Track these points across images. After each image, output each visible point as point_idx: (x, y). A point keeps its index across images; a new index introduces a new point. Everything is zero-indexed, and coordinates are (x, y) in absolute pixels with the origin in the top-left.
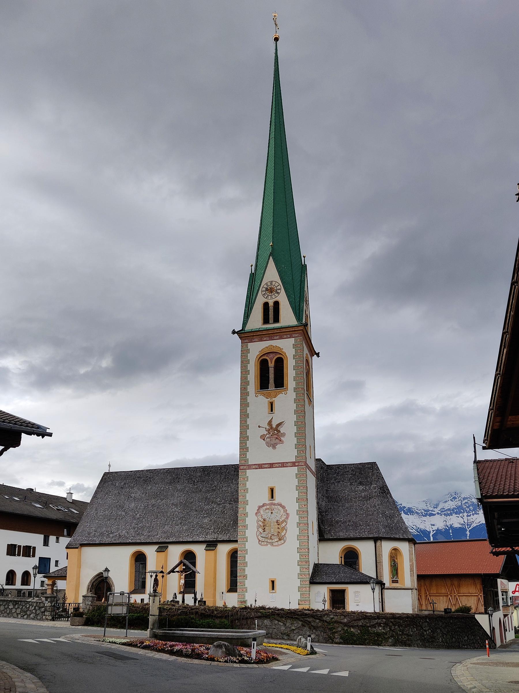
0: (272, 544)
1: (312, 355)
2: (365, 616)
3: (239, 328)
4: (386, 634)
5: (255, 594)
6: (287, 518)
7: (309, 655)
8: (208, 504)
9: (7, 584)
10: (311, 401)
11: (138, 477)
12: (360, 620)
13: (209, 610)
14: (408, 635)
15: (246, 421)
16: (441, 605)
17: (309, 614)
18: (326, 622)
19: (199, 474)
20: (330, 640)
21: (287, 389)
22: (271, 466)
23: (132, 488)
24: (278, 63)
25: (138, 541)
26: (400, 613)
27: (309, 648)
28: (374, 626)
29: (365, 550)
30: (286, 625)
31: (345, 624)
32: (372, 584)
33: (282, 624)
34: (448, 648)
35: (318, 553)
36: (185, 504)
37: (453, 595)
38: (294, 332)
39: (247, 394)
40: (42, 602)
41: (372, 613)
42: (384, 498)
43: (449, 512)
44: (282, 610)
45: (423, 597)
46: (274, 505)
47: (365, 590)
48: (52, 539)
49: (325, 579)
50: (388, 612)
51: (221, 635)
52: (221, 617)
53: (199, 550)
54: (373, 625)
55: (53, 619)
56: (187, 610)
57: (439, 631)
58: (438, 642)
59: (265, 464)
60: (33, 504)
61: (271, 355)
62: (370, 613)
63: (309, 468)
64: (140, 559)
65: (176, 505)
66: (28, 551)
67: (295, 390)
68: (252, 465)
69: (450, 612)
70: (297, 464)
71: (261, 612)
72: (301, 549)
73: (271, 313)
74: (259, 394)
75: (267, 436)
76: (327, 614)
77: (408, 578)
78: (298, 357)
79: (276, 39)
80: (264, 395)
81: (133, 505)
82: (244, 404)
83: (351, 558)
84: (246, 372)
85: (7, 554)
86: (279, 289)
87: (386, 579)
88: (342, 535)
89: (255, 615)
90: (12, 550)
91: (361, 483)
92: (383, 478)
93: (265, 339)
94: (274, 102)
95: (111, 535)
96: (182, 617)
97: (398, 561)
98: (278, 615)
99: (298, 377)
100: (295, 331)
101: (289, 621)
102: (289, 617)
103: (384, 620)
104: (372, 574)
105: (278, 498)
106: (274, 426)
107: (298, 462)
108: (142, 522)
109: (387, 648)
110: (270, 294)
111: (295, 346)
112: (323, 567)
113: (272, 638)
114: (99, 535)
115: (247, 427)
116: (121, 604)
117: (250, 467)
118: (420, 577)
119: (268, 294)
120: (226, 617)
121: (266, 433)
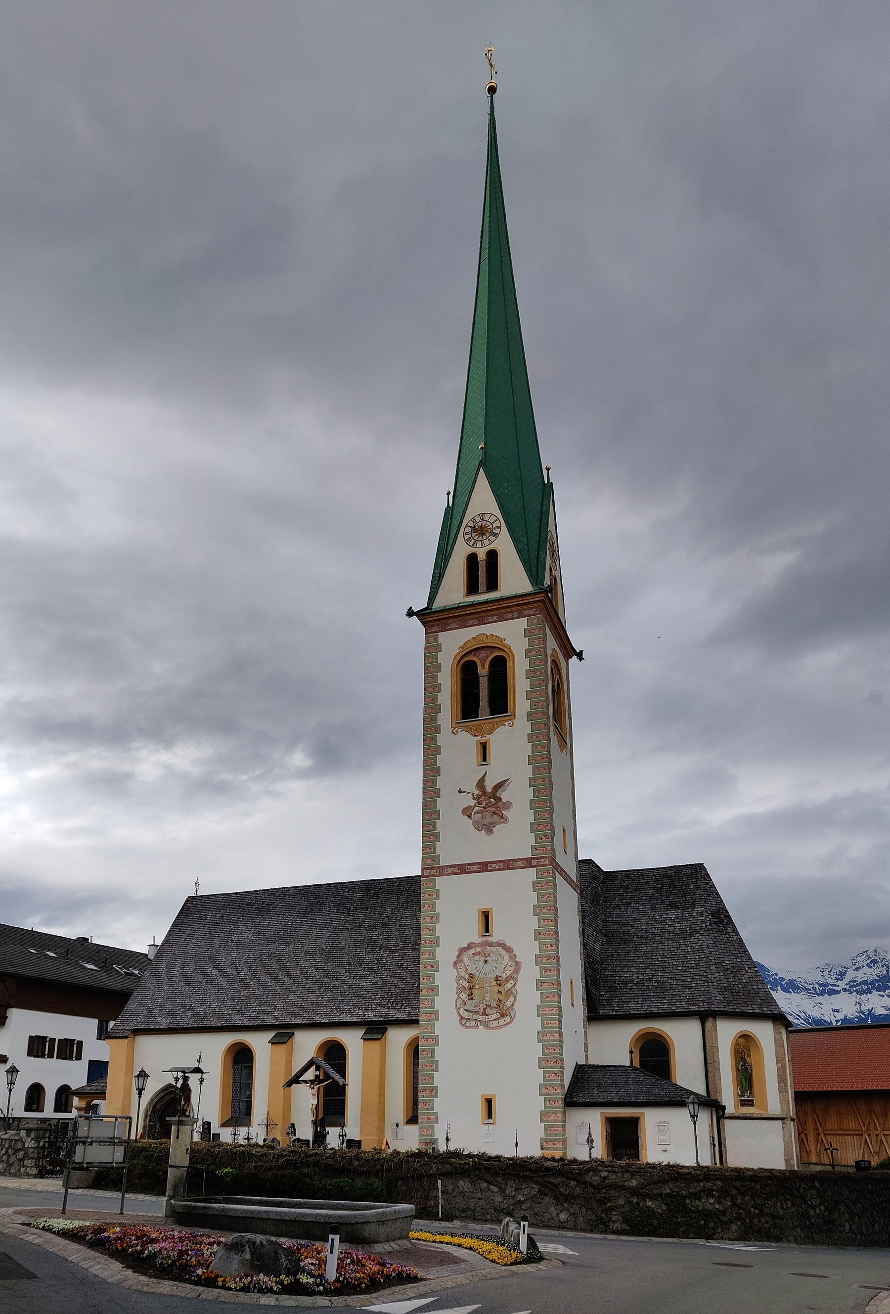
0: (487, 1025)
1: (568, 657)
2: (678, 1173)
3: (420, 604)
4: (724, 1213)
5: (460, 1130)
6: (517, 971)
7: (520, 1263)
8: (373, 951)
9: (28, 1109)
10: (565, 742)
11: (247, 904)
12: (665, 1182)
13: (342, 1158)
14: (773, 1217)
15: (434, 782)
16: (849, 1153)
17: (554, 1168)
18: (591, 1185)
19: (359, 895)
20: (600, 1225)
21: (513, 716)
22: (484, 867)
23: (234, 924)
24: (495, 129)
25: (238, 1023)
26: (755, 1167)
27: (523, 1245)
28: (696, 1196)
29: (683, 1037)
30: (504, 1192)
31: (633, 1192)
32: (691, 1106)
33: (496, 1190)
34: (865, 1246)
35: (586, 1045)
36: (330, 952)
37: (873, 1133)
38: (526, 607)
39: (437, 729)
40: (21, 1139)
41: (693, 1168)
42: (721, 932)
43: (865, 988)
44: (498, 1158)
45: (811, 1137)
46: (491, 945)
47: (678, 1117)
49: (597, 1096)
50: (651, 1161)
51: (304, 1215)
52: (367, 1174)
53: (352, 1041)
54: (695, 1194)
55: (41, 1175)
56: (239, 1156)
57: (842, 1208)
58: (841, 1232)
59: (473, 864)
60: (81, 963)
61: (483, 654)
62: (688, 1167)
63: (562, 872)
64: (241, 1058)
65: (313, 954)
66: (69, 1049)
67: (530, 716)
68: (447, 867)
69: (868, 1169)
70: (534, 863)
71: (450, 1164)
72: (545, 1034)
73: (482, 572)
74: (459, 727)
75: (476, 809)
76: (595, 1170)
77: (774, 1095)
78: (534, 652)
79: (492, 90)
80: (469, 730)
81: (234, 955)
82: (431, 750)
83: (654, 1055)
84: (434, 687)
85: (29, 1054)
86: (496, 528)
87: (728, 1098)
88: (633, 1007)
89: (438, 1169)
90: (38, 1046)
91: (673, 906)
92: (717, 894)
93: (470, 622)
94: (488, 197)
95: (190, 1013)
96: (287, 1172)
97: (753, 1060)
98: (488, 1169)
99: (535, 692)
100: (528, 603)
101: (510, 1183)
102: (510, 1174)
103: (719, 1183)
104: (700, 1088)
105: (498, 932)
106: (489, 789)
107: (538, 858)
108: (247, 986)
109: (726, 1245)
110: (480, 539)
111: (528, 633)
112: (595, 1072)
113: (475, 1220)
114: (168, 1014)
115: (437, 793)
116: (112, 1142)
117: (442, 871)
118: (800, 1097)
119: (476, 538)
120: (377, 1174)
121: (473, 803)
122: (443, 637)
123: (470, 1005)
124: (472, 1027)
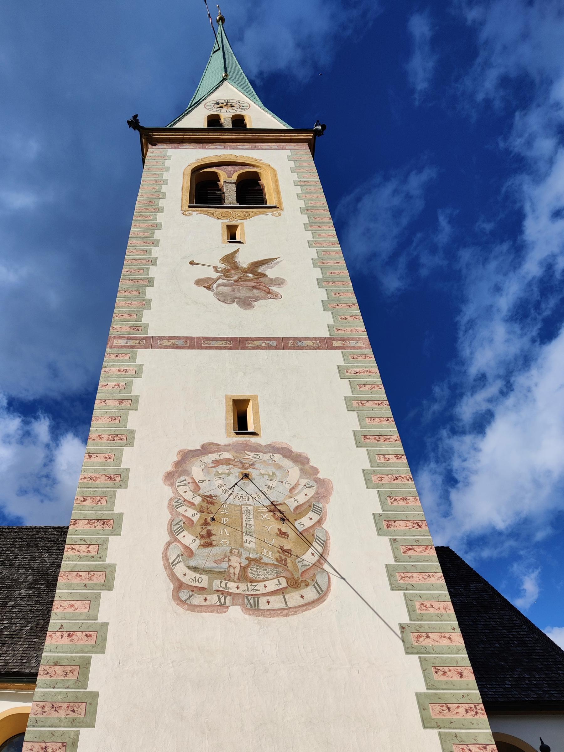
0: (252, 605)
123: (205, 557)
124: (211, 608)
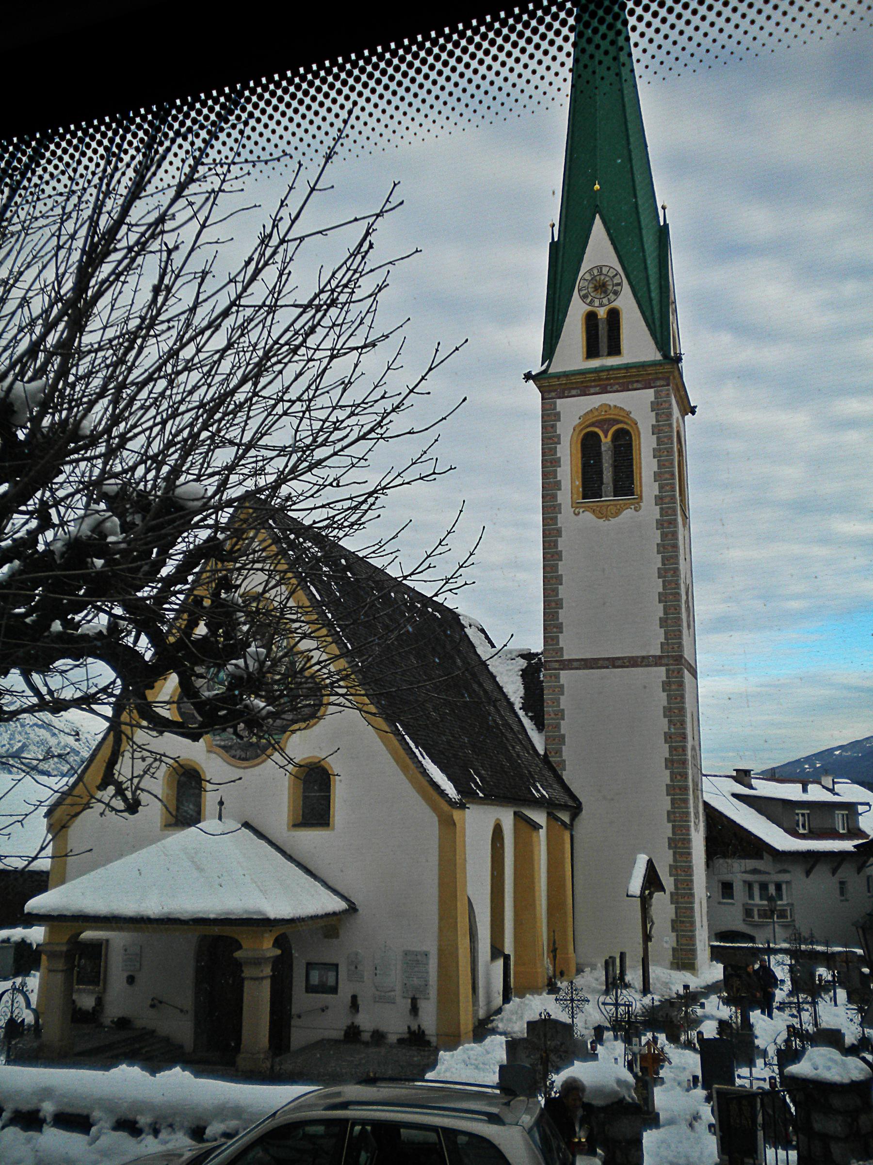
3: (536, 369)
48: (681, 991)
73: (603, 335)
117: (568, 665)
122: (562, 404)
